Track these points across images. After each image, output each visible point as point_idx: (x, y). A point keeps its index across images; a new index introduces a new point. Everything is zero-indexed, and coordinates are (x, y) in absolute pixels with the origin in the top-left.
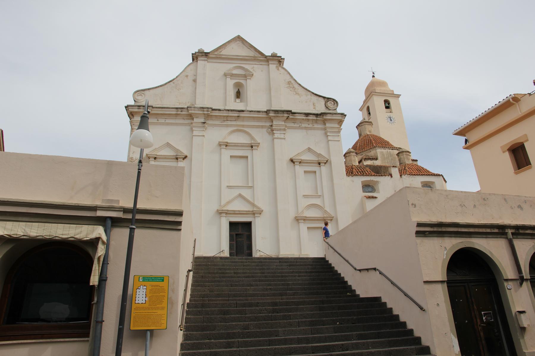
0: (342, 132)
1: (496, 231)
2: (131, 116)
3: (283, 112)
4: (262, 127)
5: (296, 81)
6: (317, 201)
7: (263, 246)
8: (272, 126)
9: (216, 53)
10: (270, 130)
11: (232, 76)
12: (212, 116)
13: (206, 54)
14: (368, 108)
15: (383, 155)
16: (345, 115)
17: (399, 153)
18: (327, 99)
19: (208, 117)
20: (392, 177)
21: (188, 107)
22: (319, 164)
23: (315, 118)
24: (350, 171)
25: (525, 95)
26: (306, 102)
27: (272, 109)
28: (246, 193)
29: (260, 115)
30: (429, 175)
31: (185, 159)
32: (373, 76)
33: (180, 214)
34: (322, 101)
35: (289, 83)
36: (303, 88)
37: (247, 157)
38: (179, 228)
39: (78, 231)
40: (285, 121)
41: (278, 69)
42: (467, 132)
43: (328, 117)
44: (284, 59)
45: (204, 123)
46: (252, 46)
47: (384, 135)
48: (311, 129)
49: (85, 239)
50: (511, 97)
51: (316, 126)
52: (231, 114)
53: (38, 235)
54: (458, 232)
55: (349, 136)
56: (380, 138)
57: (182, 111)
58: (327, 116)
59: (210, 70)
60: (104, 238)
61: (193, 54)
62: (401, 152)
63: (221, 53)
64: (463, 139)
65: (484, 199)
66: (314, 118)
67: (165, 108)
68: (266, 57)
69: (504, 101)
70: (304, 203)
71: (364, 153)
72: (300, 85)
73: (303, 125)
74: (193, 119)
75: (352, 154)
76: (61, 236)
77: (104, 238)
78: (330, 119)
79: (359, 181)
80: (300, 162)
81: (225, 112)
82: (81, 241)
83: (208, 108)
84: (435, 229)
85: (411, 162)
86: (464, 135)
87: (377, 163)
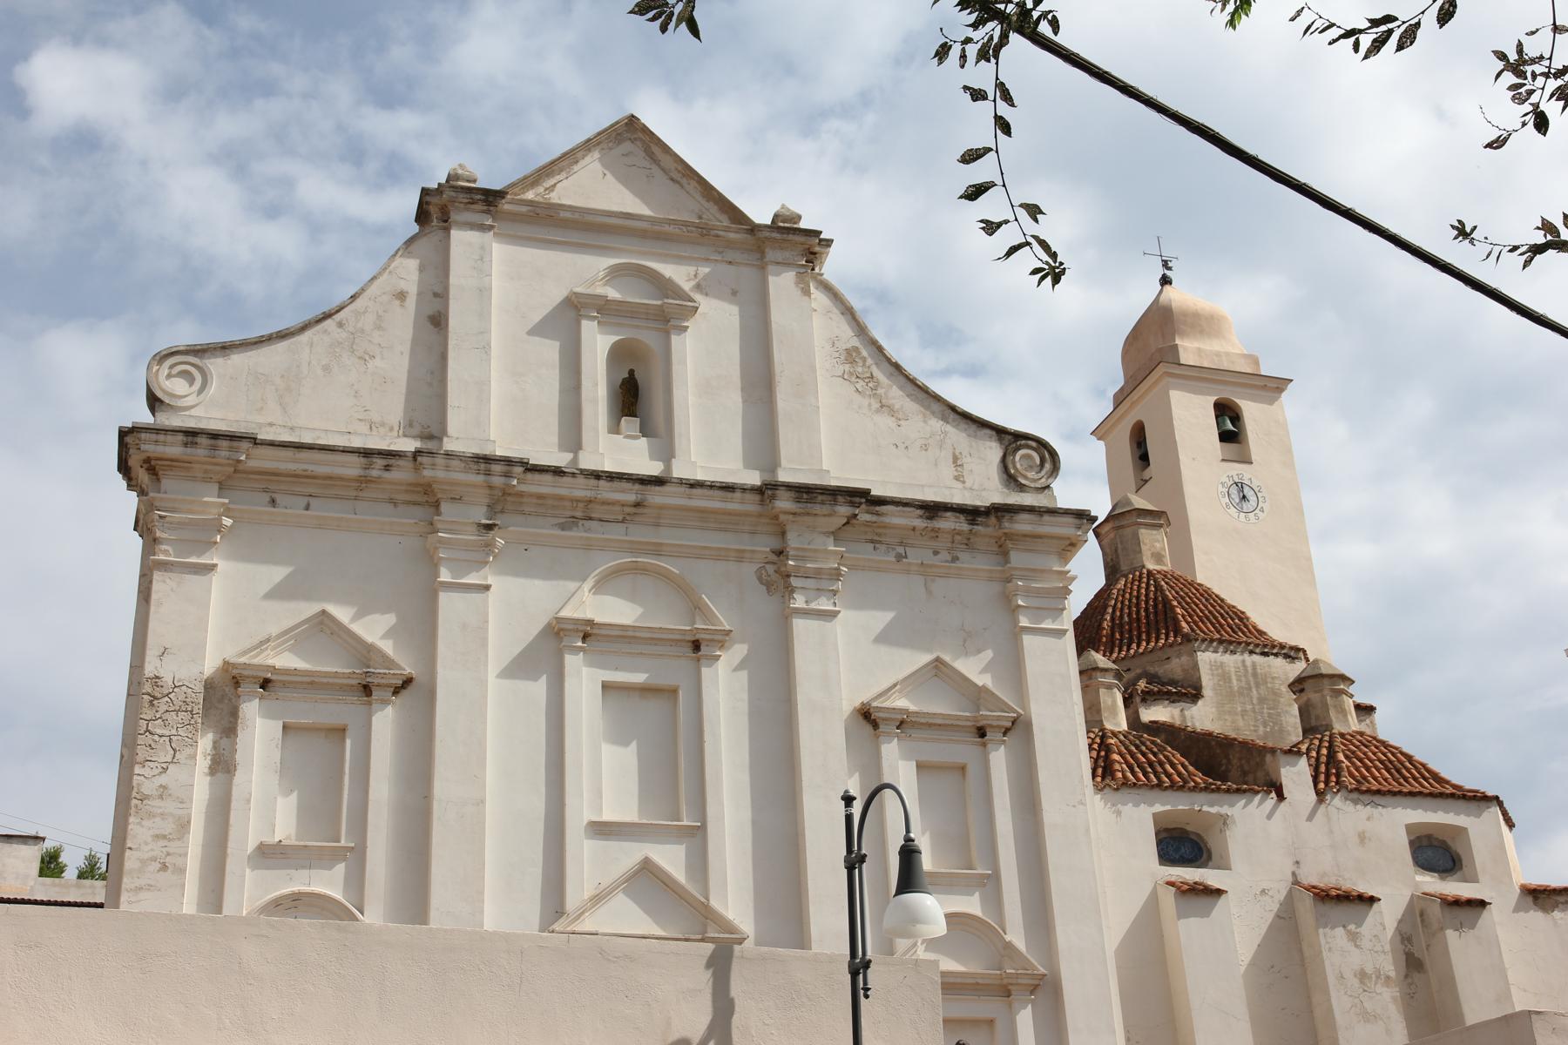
4: (740, 556)
5: (880, 349)
8: (780, 553)
9: (530, 195)
11: (606, 311)
12: (521, 495)
13: (491, 198)
14: (1139, 437)
15: (1225, 677)
18: (1011, 440)
19: (502, 503)
20: (1281, 797)
21: (417, 453)
22: (981, 732)
23: (965, 527)
26: (925, 448)
28: (671, 859)
29: (734, 504)
30: (1441, 795)
31: (404, 693)
32: (1165, 281)
35: (851, 356)
37: (673, 692)
40: (836, 535)
41: (807, 292)
43: (1023, 524)
44: (828, 243)
45: (489, 527)
46: (687, 174)
48: (946, 576)
51: (967, 560)
52: (606, 491)
57: (387, 468)
59: (504, 281)
62: (1317, 686)
63: (555, 197)
68: (753, 228)
74: (436, 505)
81: (581, 480)
83: (509, 461)
87: (1202, 717)
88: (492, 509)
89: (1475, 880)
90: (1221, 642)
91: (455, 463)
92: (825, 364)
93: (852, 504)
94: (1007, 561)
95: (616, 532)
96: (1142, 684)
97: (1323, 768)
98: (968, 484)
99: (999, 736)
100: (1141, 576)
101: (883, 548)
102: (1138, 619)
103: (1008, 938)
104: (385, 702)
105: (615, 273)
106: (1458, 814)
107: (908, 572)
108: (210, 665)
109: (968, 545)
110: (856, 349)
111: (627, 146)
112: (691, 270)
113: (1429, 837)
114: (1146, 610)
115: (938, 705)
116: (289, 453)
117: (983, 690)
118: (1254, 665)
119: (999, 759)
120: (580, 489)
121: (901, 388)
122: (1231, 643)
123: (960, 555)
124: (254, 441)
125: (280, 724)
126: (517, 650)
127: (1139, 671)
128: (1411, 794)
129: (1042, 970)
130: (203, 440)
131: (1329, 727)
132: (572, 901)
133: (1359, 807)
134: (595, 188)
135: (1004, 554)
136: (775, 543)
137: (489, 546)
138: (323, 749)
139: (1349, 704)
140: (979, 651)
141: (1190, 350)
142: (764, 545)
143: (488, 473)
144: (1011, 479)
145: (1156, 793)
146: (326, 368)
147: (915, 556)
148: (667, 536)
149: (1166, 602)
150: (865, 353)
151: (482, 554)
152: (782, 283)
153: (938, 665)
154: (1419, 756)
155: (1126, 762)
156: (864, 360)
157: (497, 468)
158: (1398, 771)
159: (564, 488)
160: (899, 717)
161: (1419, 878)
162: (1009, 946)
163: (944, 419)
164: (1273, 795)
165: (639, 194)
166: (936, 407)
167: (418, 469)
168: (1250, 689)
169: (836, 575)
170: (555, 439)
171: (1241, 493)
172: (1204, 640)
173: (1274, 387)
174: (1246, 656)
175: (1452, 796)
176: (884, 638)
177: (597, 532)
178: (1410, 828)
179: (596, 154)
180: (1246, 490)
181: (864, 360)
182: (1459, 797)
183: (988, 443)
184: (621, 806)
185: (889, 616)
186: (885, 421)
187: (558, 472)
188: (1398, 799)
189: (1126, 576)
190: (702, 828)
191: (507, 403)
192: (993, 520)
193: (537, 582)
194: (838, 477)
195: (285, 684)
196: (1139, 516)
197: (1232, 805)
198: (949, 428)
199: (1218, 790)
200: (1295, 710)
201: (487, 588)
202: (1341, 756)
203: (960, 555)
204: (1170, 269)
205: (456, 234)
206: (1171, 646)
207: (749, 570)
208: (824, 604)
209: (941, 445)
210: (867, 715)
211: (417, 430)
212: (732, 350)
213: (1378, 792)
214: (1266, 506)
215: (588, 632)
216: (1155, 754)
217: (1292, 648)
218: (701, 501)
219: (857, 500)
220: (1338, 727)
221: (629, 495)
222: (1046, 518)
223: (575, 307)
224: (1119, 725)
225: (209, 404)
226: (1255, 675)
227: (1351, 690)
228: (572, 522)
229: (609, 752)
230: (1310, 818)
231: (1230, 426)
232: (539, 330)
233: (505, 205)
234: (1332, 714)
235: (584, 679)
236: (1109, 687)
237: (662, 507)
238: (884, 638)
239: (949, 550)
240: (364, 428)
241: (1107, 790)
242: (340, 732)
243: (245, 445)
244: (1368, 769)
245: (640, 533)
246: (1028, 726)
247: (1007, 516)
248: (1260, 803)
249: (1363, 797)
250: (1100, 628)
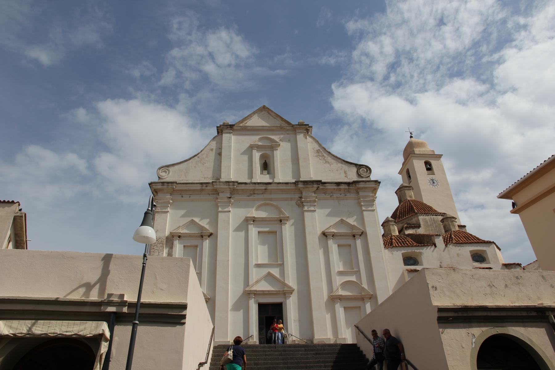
1: (534, 314)
2: (155, 193)
3: (313, 182)
4: (291, 199)
5: (325, 149)
7: (292, 330)
9: (241, 125)
10: (299, 202)
11: (258, 148)
12: (238, 190)
13: (231, 127)
14: (408, 172)
15: (426, 222)
16: (380, 183)
17: (443, 219)
18: (359, 167)
19: (233, 192)
20: (435, 246)
21: (213, 182)
22: (354, 236)
23: (347, 187)
24: (389, 242)
26: (337, 170)
27: (301, 180)
28: (275, 272)
29: (289, 187)
30: (478, 243)
32: (411, 137)
33: (184, 307)
34: (355, 170)
35: (318, 151)
37: (276, 232)
38: (183, 321)
39: (82, 327)
40: (315, 192)
41: (306, 138)
42: (513, 195)
43: (361, 185)
44: (311, 127)
45: (230, 198)
47: (427, 200)
49: (89, 336)
51: (348, 195)
52: (257, 187)
53: (42, 333)
54: (487, 316)
55: (386, 203)
56: (423, 204)
57: (206, 186)
59: (234, 143)
60: (108, 334)
61: (217, 127)
62: (447, 220)
63: (247, 125)
64: (509, 202)
65: (517, 278)
67: (189, 183)
68: (293, 126)
70: (338, 281)
74: (218, 194)
76: (65, 333)
77: (108, 334)
78: (363, 188)
81: (251, 185)
82: (85, 338)
83: (233, 182)
84: (460, 314)
85: (457, 228)
86: (511, 198)
87: (421, 231)
88: (231, 194)
89: (490, 263)
91: (221, 184)
92: (311, 154)
93: (318, 184)
95: (261, 196)
96: (406, 225)
104: (206, 239)
105: (261, 139)
108: (167, 233)
111: (263, 112)
112: (279, 136)
113: (476, 253)
115: (343, 230)
116: (184, 185)
117: (354, 226)
119: (359, 242)
120: (252, 187)
124: (176, 183)
125: (183, 246)
126: (238, 225)
129: (372, 293)
130: (165, 184)
131: (451, 230)
132: (250, 283)
134: (256, 121)
135: (358, 193)
136: (300, 195)
137: (230, 202)
138: (193, 250)
139: (456, 224)
141: (417, 151)
142: (297, 196)
143: (229, 185)
144: (359, 175)
145: (402, 248)
146: (195, 167)
147: (335, 196)
148: (273, 196)
149: (412, 206)
151: (228, 204)
152: (300, 137)
153: (342, 220)
157: (231, 184)
159: (247, 187)
162: (363, 288)
163: (342, 163)
165: (267, 122)
166: (339, 161)
167: (213, 185)
169: (315, 201)
170: (247, 177)
171: (433, 181)
173: (440, 156)
174: (431, 216)
177: (256, 197)
178: (471, 252)
179: (256, 115)
184: (263, 259)
185: (329, 210)
186: (327, 165)
187: (246, 183)
190: (283, 264)
191: (234, 170)
193: (242, 209)
194: (314, 178)
195: (184, 237)
197: (423, 249)
198: (343, 165)
199: (419, 246)
200: (442, 226)
201: (230, 211)
205: (224, 135)
207: (294, 202)
208: (312, 209)
211: (215, 178)
212: (289, 154)
213: (461, 243)
215: (254, 220)
218: (280, 187)
220: (453, 230)
221: (263, 187)
223: (252, 147)
225: (169, 177)
226: (434, 220)
227: (456, 220)
228: (251, 195)
229: (260, 248)
230: (444, 251)
232: (244, 153)
233: (235, 128)
234: (451, 227)
235: (253, 231)
236: (393, 225)
237: (272, 190)
240: (203, 179)
242: (196, 246)
243: (174, 184)
245: (266, 196)
246: (366, 233)
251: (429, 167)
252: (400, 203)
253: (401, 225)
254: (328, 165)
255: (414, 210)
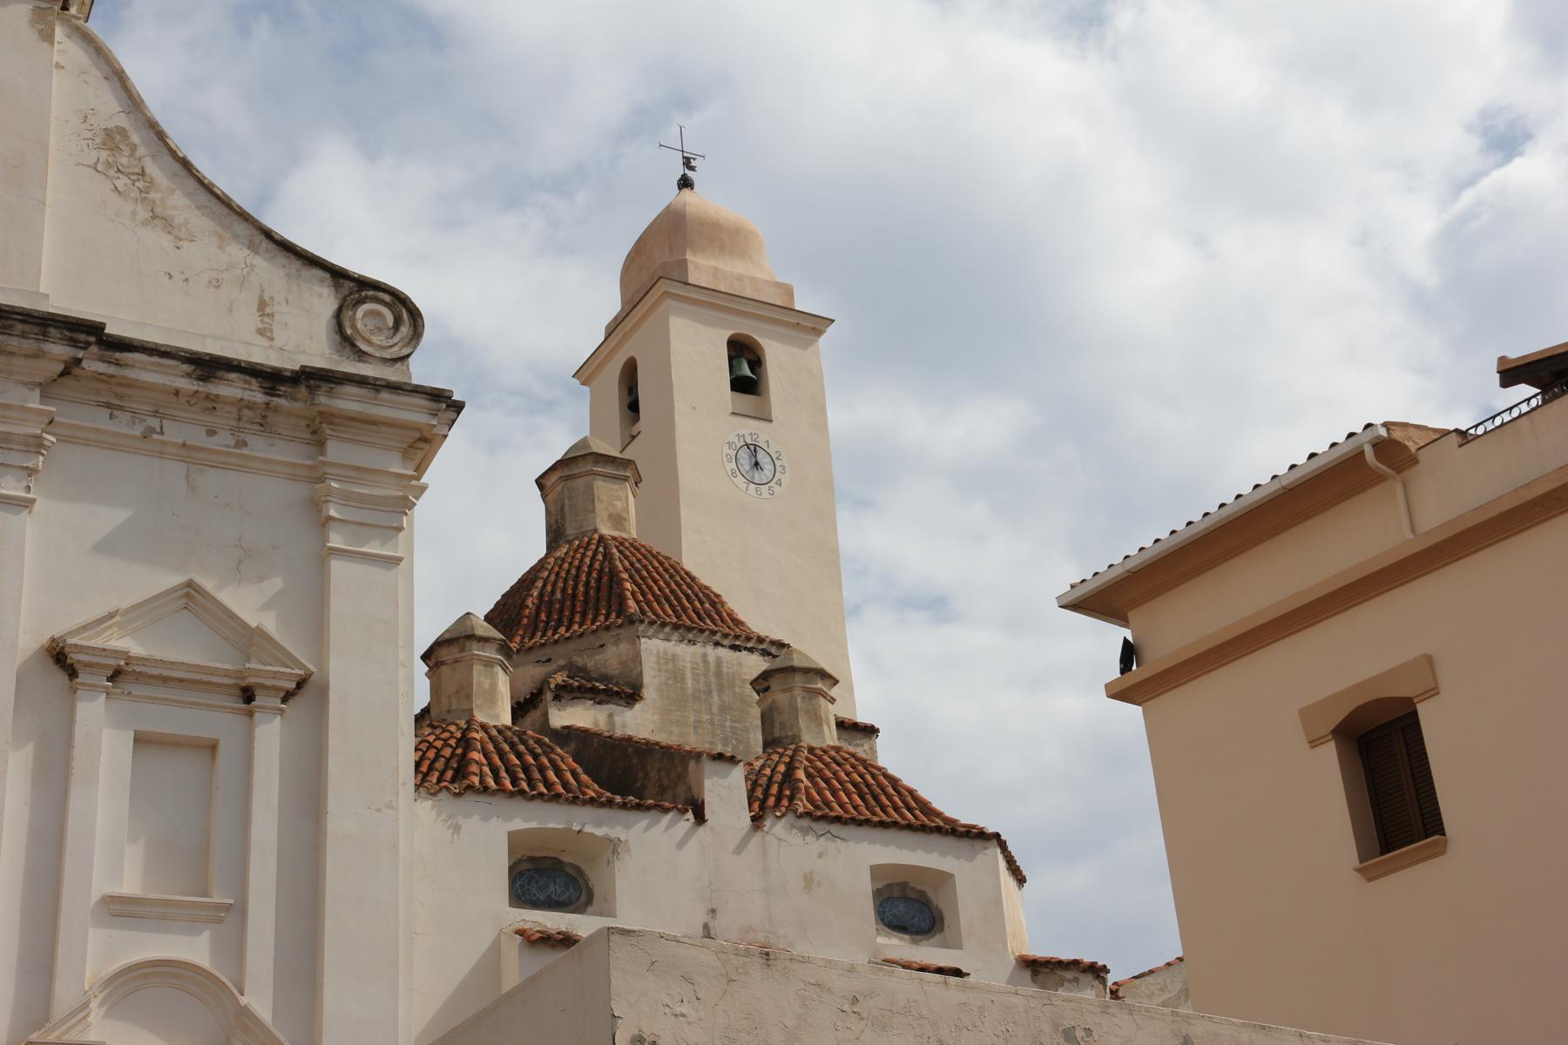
0: (423, 510)
5: (161, 135)
6: (194, 949)
14: (630, 374)
15: (677, 675)
16: (458, 407)
17: (766, 675)
18: (355, 289)
20: (700, 818)
22: (248, 695)
23: (260, 398)
24: (449, 760)
25: (1446, 433)
26: (216, 284)
30: (923, 828)
32: (685, 183)
34: (324, 301)
35: (112, 139)
36: (209, 188)
40: (46, 389)
41: (48, 37)
42: (1137, 603)
43: (348, 401)
47: (705, 555)
48: (224, 467)
50: (1370, 435)
51: (258, 447)
55: (473, 533)
58: (340, 396)
64: (1114, 636)
66: (255, 394)
69: (1337, 452)
71: (560, 649)
72: (186, 164)
73: (174, 433)
75: (477, 650)
78: (353, 419)
79: (488, 834)
80: (116, 675)
85: (831, 737)
86: (1119, 618)
90: (676, 627)
93: (73, 343)
94: (323, 453)
96: (560, 678)
97: (774, 789)
98: (278, 342)
99: (276, 702)
100: (588, 543)
101: (126, 416)
102: (574, 596)
103: (244, 1000)
106: (943, 854)
107: (161, 455)
109: (264, 425)
110: (122, 132)
113: (903, 886)
114: (587, 583)
117: (260, 632)
118: (719, 662)
121: (188, 195)
122: (689, 629)
123: (250, 439)
127: (562, 662)
128: (882, 825)
131: (796, 739)
133: (810, 838)
135: (318, 442)
140: (261, 579)
141: (702, 268)
144: (346, 341)
149: (614, 573)
150: (135, 138)
153: (191, 594)
154: (908, 780)
155: (491, 764)
156: (133, 148)
158: (876, 798)
160: (112, 662)
161: (881, 940)
162: (245, 1012)
163: (252, 247)
164: (690, 815)
166: (241, 228)
168: (709, 693)
172: (652, 623)
174: (710, 649)
175: (938, 830)
176: (106, 547)
178: (876, 871)
180: (761, 455)
181: (133, 148)
182: (946, 833)
183: (317, 289)
186: (157, 238)
188: (864, 831)
189: (570, 542)
192: (303, 390)
196: (596, 463)
197: (628, 827)
198: (259, 262)
199: (610, 803)
200: (756, 712)
202: (801, 774)
203: (250, 439)
204: (692, 169)
206: (607, 628)
209: (242, 283)
210: (60, 657)
214: (785, 479)
216: (536, 757)
217: (773, 643)
219: (82, 337)
220: (808, 739)
222: (385, 395)
224: (497, 717)
226: (719, 674)
227: (834, 692)
230: (739, 850)
231: (746, 371)
236: (489, 663)
238: (106, 547)
239: (233, 431)
241: (443, 795)
244: (834, 793)
246: (324, 691)
247: (325, 386)
248: (670, 825)
249: (815, 825)
250: (523, 606)
251: (747, 372)
252: (552, 544)
253: (532, 673)
254: (166, 241)
255: (622, 600)
